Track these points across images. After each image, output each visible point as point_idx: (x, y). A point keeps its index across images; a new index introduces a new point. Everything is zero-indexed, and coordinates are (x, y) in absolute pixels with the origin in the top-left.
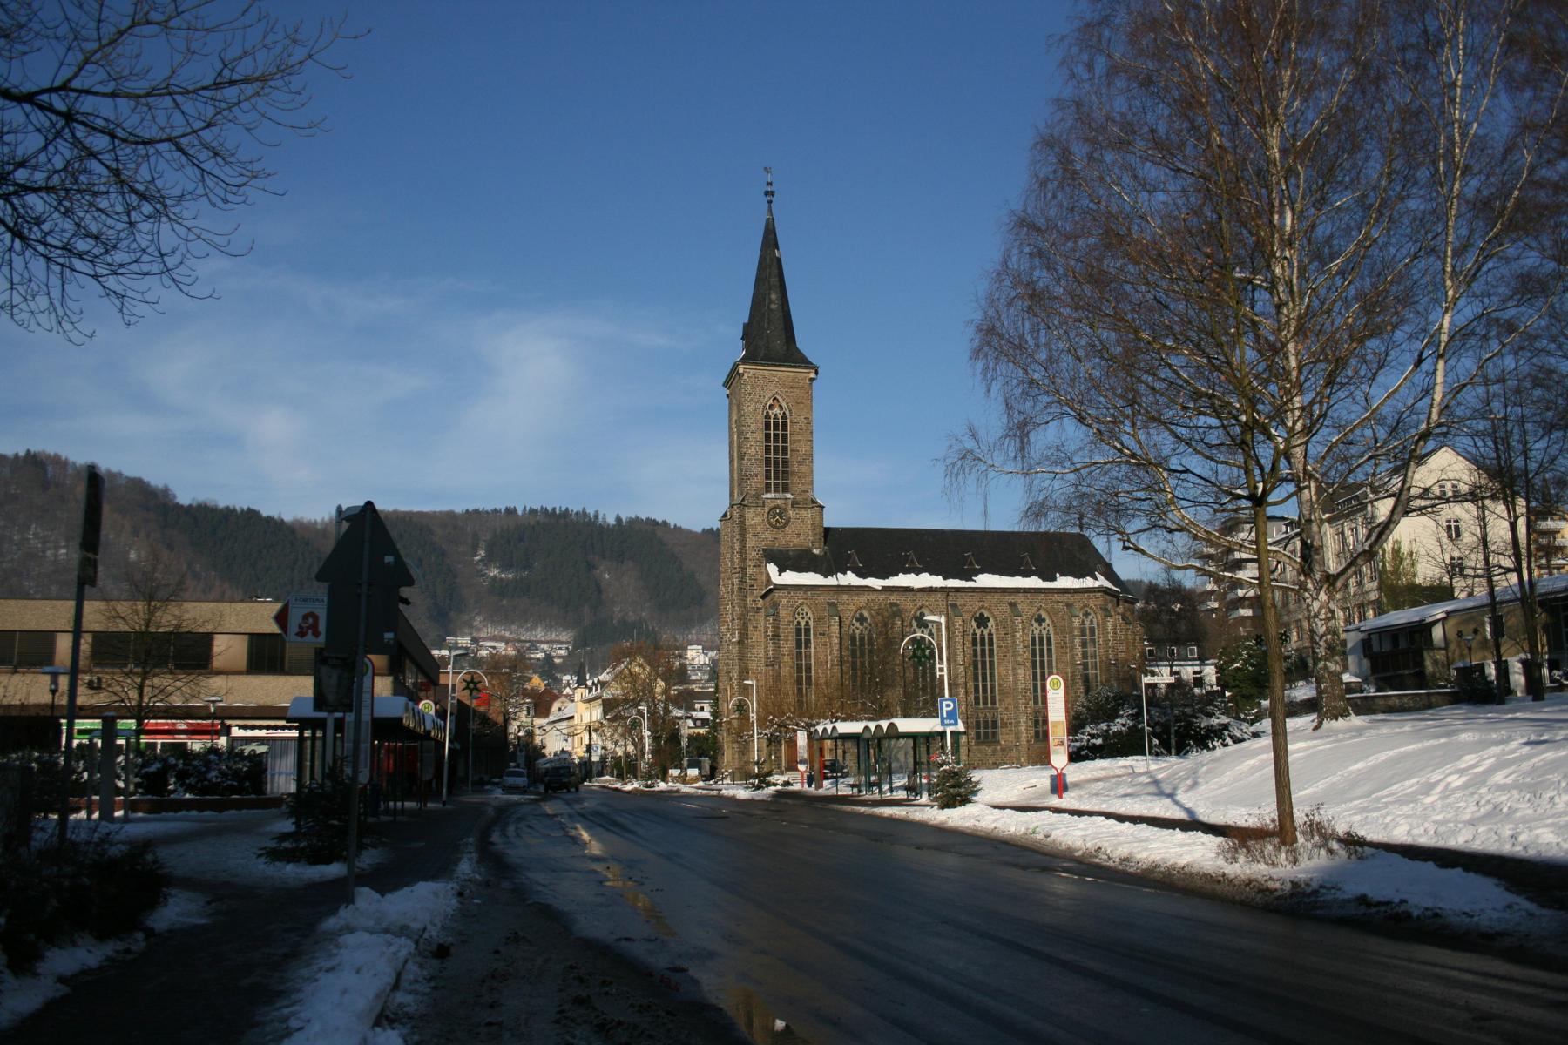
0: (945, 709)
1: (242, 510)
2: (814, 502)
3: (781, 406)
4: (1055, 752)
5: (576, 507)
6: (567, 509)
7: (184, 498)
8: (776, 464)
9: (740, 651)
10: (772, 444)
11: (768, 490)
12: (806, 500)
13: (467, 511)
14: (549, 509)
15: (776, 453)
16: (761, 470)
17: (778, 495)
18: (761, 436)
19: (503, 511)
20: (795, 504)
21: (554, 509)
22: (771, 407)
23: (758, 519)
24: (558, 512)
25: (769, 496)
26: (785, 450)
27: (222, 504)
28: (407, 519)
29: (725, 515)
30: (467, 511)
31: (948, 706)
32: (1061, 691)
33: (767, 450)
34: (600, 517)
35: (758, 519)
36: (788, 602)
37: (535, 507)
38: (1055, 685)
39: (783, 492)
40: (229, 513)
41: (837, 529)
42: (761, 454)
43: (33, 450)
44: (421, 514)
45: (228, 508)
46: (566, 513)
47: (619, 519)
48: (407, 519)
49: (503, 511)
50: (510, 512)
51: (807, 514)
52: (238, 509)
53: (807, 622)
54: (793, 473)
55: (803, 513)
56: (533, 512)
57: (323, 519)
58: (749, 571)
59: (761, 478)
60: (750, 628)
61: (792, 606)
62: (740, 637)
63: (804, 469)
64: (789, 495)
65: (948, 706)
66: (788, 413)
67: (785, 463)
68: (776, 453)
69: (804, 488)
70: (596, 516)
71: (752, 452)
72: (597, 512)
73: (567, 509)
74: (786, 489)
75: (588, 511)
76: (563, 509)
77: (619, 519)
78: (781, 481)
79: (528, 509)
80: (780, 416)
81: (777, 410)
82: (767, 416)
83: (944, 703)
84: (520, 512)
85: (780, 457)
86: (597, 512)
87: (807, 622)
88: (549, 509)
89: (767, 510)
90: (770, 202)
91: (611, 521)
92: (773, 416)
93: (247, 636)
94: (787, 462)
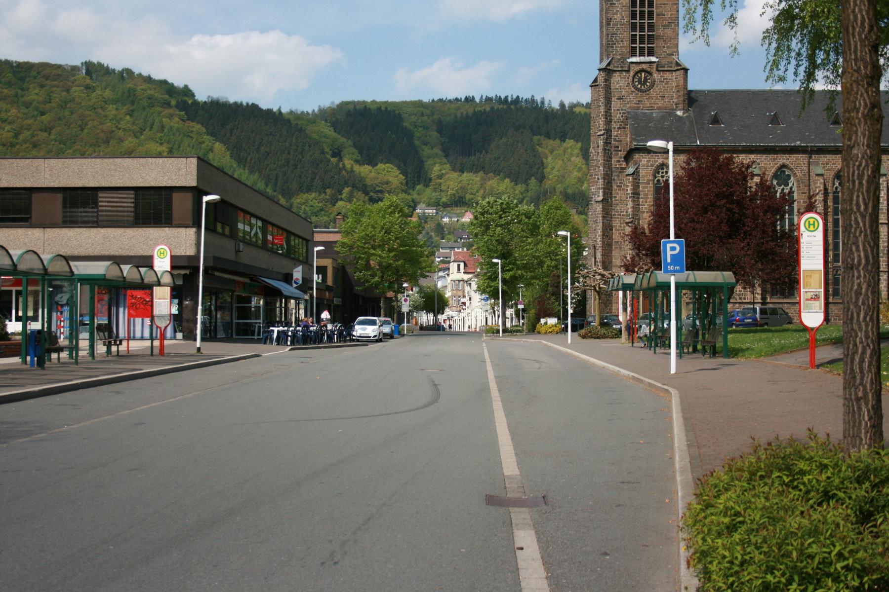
0: (669, 253)
1: (247, 104)
2: (678, 64)
4: (806, 306)
5: (525, 95)
6: (518, 97)
7: (201, 96)
8: (642, 29)
9: (604, 209)
10: (646, 9)
11: (633, 53)
12: (671, 63)
13: (433, 100)
14: (503, 97)
15: (642, 17)
16: (626, 35)
17: (642, 59)
19: (463, 100)
20: (659, 68)
21: (506, 97)
23: (623, 83)
24: (510, 99)
25: (634, 59)
26: (651, 14)
27: (232, 100)
28: (383, 109)
29: (595, 80)
30: (433, 100)
31: (673, 249)
32: (819, 234)
33: (633, 15)
34: (546, 103)
35: (623, 83)
36: (648, 161)
37: (490, 96)
38: (812, 226)
39: (648, 55)
40: (237, 106)
41: (704, 91)
42: (627, 19)
43: (322, 106)
44: (394, 104)
45: (236, 103)
46: (517, 101)
47: (562, 105)
48: (383, 109)
49: (463, 100)
50: (469, 100)
51: (675, 78)
52: (245, 104)
54: (659, 37)
55: (668, 75)
56: (489, 99)
57: (314, 111)
58: (614, 133)
59: (627, 43)
60: (614, 187)
61: (652, 165)
62: (604, 195)
63: (669, 32)
64: (653, 59)
65: (673, 249)
67: (651, 27)
68: (642, 17)
69: (669, 51)
70: (543, 103)
71: (617, 17)
72: (543, 99)
73: (518, 97)
74: (651, 53)
75: (535, 98)
76: (514, 97)
77: (562, 105)
78: (637, 45)
79: (484, 97)
83: (669, 246)
84: (477, 100)
85: (646, 21)
86: (543, 99)
88: (503, 97)
89: (632, 73)
91: (556, 105)
93: (131, 194)
94: (653, 26)
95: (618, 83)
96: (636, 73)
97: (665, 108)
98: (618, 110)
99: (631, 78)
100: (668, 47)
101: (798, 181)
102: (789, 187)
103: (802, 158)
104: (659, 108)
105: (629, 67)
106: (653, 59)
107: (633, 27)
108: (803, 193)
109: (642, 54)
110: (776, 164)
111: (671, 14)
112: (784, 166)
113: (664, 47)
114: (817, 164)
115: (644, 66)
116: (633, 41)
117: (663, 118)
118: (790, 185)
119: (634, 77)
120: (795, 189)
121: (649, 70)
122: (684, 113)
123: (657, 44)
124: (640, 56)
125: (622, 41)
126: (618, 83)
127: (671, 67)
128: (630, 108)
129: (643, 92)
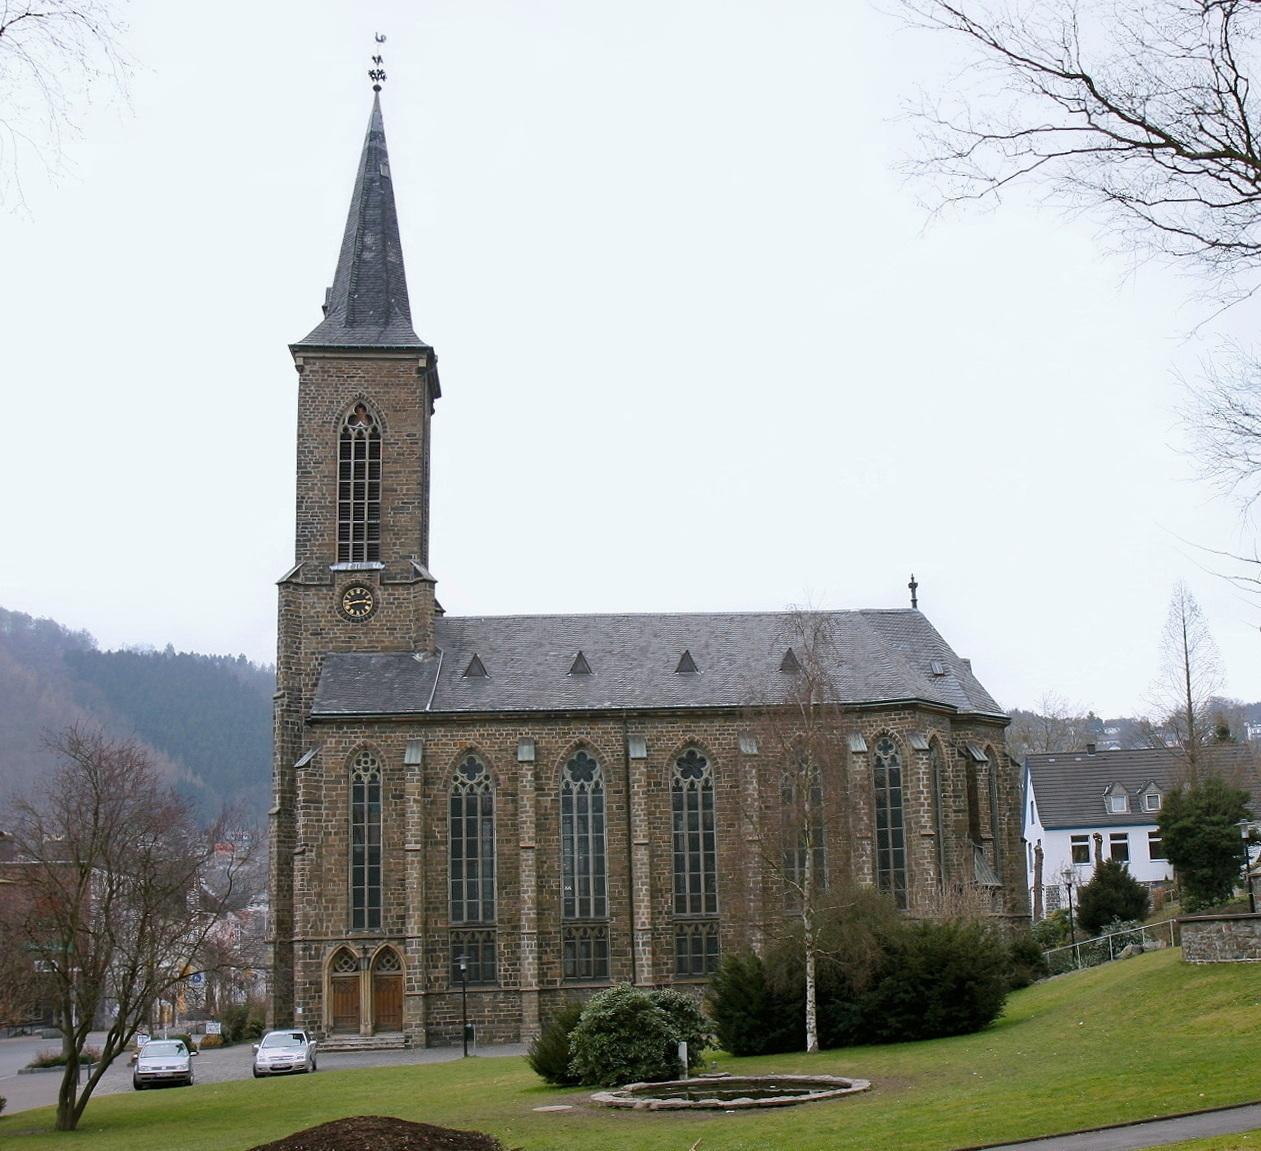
3: (369, 418)
8: (359, 514)
12: (408, 571)
22: (352, 420)
33: (344, 491)
39: (369, 560)
55: (400, 592)
64: (376, 565)
74: (373, 557)
80: (366, 434)
81: (361, 424)
89: (338, 590)
90: (377, 89)
92: (354, 434)
95: (313, 607)
97: (396, 649)
98: (313, 653)
99: (336, 599)
100: (402, 545)
101: (608, 771)
102: (592, 783)
104: (385, 649)
105: (333, 579)
106: (376, 565)
107: (344, 511)
108: (617, 792)
109: (357, 558)
110: (567, 742)
112: (581, 745)
113: (395, 544)
114: (640, 739)
115: (359, 577)
116: (343, 536)
118: (705, 776)
120: (602, 785)
121: (368, 583)
123: (385, 539)
124: (354, 560)
126: (313, 607)
127: (407, 578)
128: (334, 649)
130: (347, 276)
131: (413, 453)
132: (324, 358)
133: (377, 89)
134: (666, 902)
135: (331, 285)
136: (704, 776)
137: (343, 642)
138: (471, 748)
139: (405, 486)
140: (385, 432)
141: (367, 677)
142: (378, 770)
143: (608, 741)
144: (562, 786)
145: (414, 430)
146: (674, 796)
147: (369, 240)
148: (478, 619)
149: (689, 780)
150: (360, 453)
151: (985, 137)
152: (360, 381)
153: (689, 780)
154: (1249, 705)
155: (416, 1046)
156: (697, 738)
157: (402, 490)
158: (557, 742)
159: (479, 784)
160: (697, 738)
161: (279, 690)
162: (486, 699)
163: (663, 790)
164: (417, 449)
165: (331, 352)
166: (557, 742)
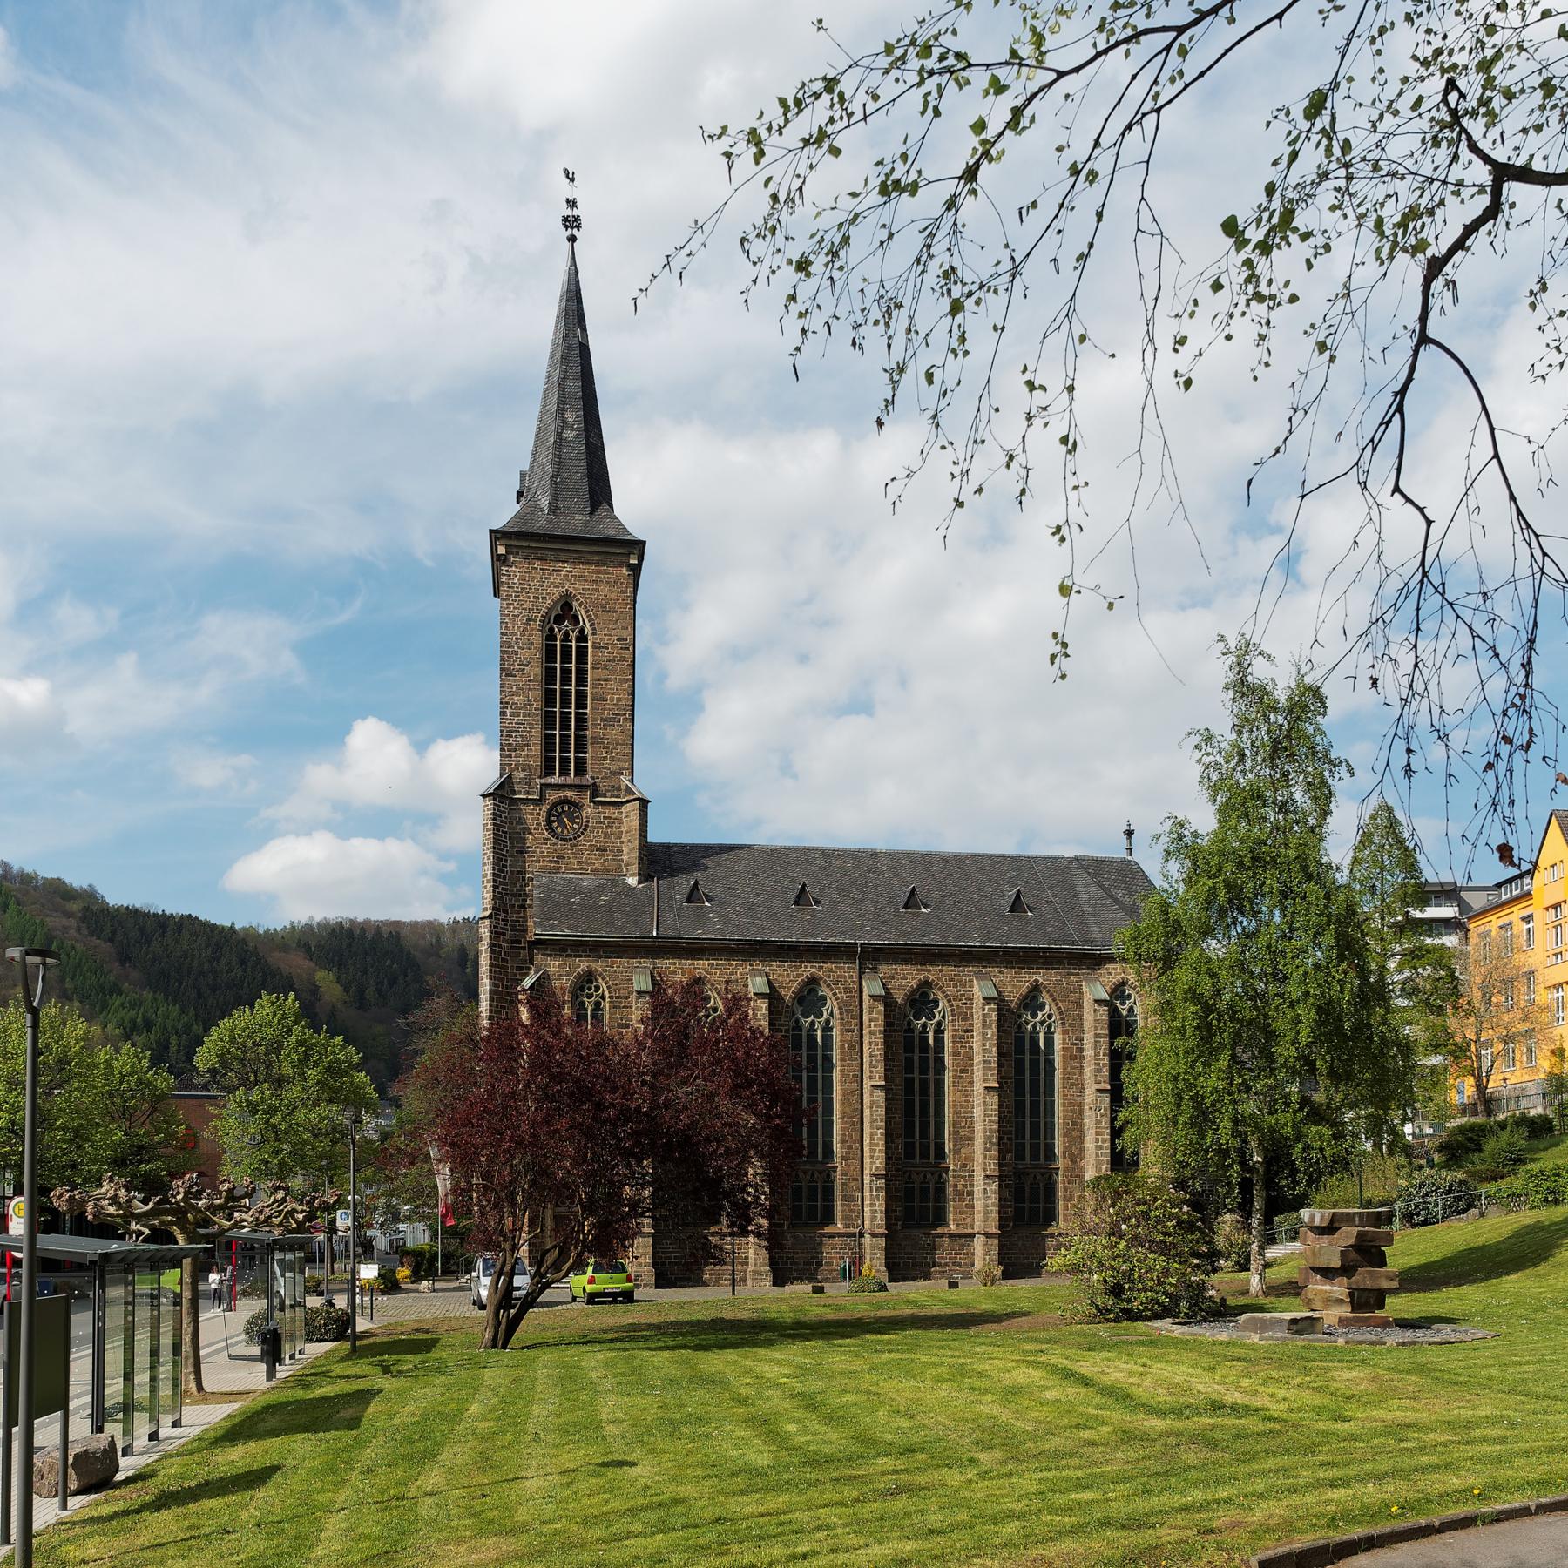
18: (536, 671)
53: (597, 1004)
66: (588, 629)
82: (551, 637)
87: (597, 1004)
89: (545, 808)
90: (572, 239)
96: (554, 805)
103: (849, 971)
110: (799, 976)
111: (619, 700)
113: (605, 759)
115: (569, 794)
117: (600, 889)
119: (549, 813)
122: (639, 882)
125: (528, 745)
127: (618, 796)
129: (566, 840)
130: (547, 459)
131: (623, 659)
132: (528, 547)
133: (572, 239)
134: (897, 1148)
135: (526, 468)
136: (937, 1018)
137: (551, 861)
138: (700, 978)
139: (614, 695)
140: (594, 634)
141: (582, 899)
142: (603, 997)
143: (841, 976)
144: (792, 1023)
145: (624, 634)
146: (905, 1037)
147: (570, 416)
148: (684, 846)
149: (810, 1020)
150: (566, 657)
151: (1357, 464)
152: (564, 578)
153: (810, 1020)
154: (463, 735)
155: (645, 1285)
156: (932, 977)
157: (612, 699)
158: (788, 975)
159: (1042, 1023)
160: (932, 977)
161: (485, 909)
162: (713, 928)
163: (896, 1031)
164: (628, 654)
165: (538, 541)
166: (788, 975)
